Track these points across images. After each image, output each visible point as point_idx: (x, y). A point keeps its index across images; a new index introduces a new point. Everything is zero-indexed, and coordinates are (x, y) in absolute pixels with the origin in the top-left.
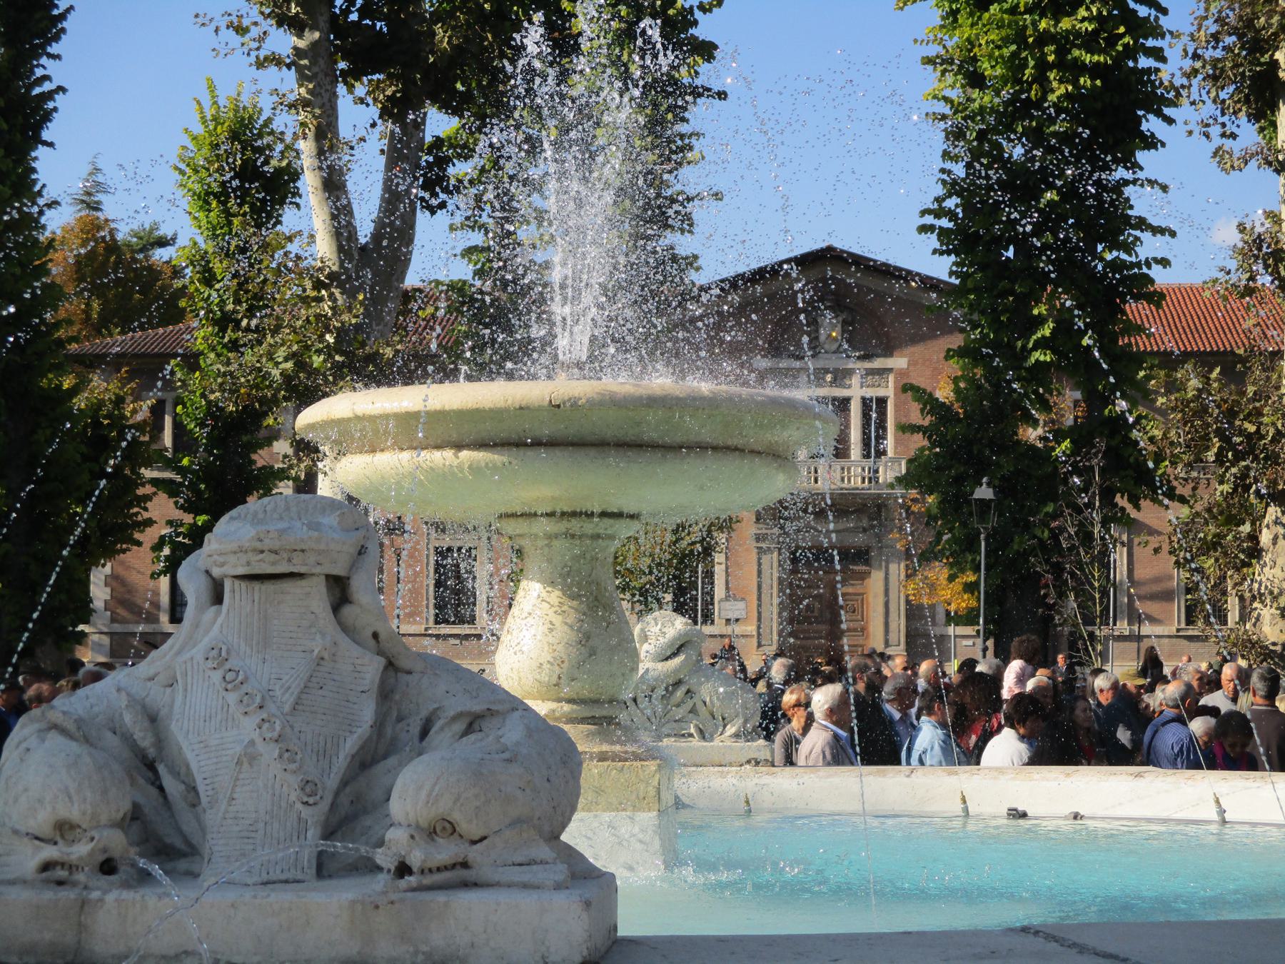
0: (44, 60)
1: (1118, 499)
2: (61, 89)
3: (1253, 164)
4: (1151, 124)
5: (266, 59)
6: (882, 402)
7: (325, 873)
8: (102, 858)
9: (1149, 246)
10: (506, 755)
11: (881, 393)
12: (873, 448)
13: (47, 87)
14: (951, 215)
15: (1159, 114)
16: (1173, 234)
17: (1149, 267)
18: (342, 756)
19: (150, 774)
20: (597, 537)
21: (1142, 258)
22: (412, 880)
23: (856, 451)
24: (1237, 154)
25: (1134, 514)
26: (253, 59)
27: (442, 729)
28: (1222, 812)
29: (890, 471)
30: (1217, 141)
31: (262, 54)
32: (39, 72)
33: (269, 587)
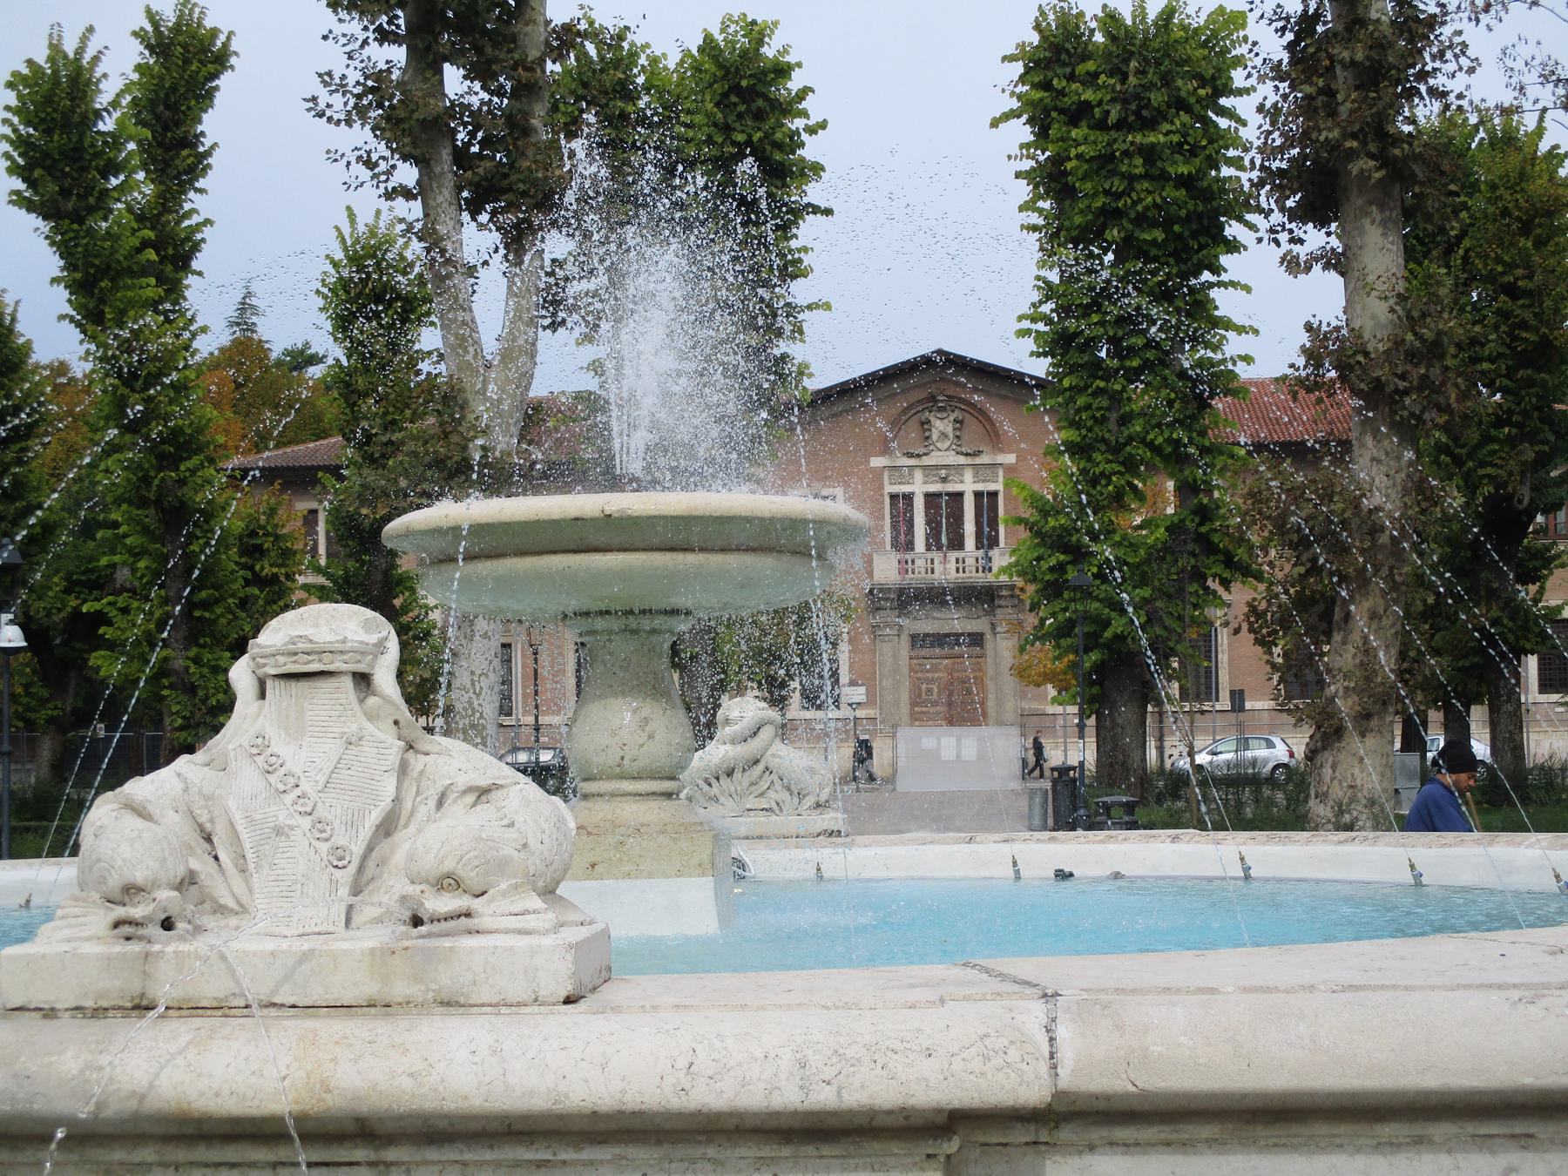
0: (191, 195)
1: (1210, 582)
2: (208, 222)
3: (1317, 268)
4: (1233, 230)
5: (394, 188)
6: (993, 495)
7: (353, 925)
8: (163, 917)
9: (1234, 345)
10: (505, 822)
11: (992, 487)
12: (987, 540)
13: (195, 219)
14: (1048, 320)
15: (1240, 219)
16: (1256, 332)
17: (1234, 364)
18: (367, 826)
19: (207, 846)
20: (654, 631)
21: (1228, 356)
22: (422, 929)
23: (970, 542)
24: (1303, 258)
25: (1225, 596)
26: (382, 191)
27: (455, 801)
28: (1247, 869)
29: (1001, 558)
30: (1285, 246)
31: (390, 185)
32: (187, 206)
33: (303, 685)
